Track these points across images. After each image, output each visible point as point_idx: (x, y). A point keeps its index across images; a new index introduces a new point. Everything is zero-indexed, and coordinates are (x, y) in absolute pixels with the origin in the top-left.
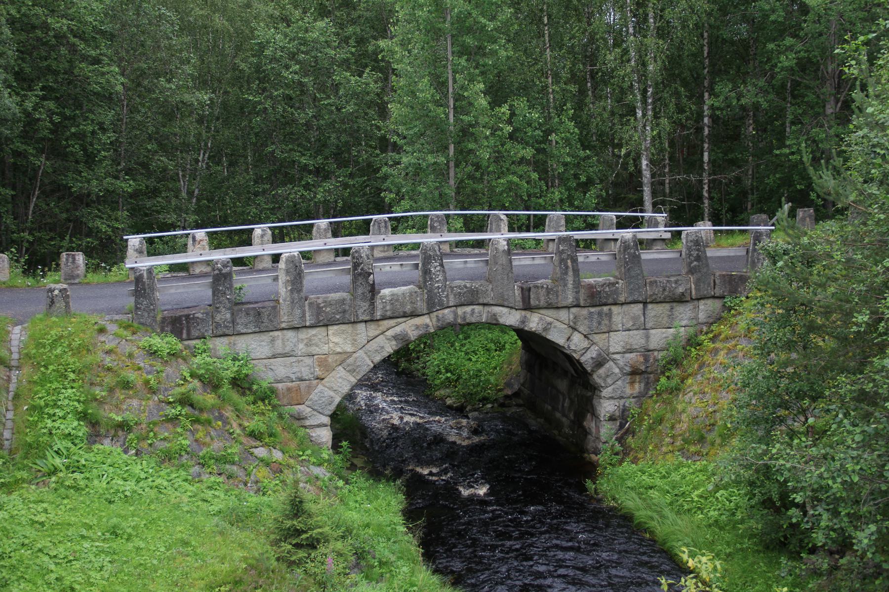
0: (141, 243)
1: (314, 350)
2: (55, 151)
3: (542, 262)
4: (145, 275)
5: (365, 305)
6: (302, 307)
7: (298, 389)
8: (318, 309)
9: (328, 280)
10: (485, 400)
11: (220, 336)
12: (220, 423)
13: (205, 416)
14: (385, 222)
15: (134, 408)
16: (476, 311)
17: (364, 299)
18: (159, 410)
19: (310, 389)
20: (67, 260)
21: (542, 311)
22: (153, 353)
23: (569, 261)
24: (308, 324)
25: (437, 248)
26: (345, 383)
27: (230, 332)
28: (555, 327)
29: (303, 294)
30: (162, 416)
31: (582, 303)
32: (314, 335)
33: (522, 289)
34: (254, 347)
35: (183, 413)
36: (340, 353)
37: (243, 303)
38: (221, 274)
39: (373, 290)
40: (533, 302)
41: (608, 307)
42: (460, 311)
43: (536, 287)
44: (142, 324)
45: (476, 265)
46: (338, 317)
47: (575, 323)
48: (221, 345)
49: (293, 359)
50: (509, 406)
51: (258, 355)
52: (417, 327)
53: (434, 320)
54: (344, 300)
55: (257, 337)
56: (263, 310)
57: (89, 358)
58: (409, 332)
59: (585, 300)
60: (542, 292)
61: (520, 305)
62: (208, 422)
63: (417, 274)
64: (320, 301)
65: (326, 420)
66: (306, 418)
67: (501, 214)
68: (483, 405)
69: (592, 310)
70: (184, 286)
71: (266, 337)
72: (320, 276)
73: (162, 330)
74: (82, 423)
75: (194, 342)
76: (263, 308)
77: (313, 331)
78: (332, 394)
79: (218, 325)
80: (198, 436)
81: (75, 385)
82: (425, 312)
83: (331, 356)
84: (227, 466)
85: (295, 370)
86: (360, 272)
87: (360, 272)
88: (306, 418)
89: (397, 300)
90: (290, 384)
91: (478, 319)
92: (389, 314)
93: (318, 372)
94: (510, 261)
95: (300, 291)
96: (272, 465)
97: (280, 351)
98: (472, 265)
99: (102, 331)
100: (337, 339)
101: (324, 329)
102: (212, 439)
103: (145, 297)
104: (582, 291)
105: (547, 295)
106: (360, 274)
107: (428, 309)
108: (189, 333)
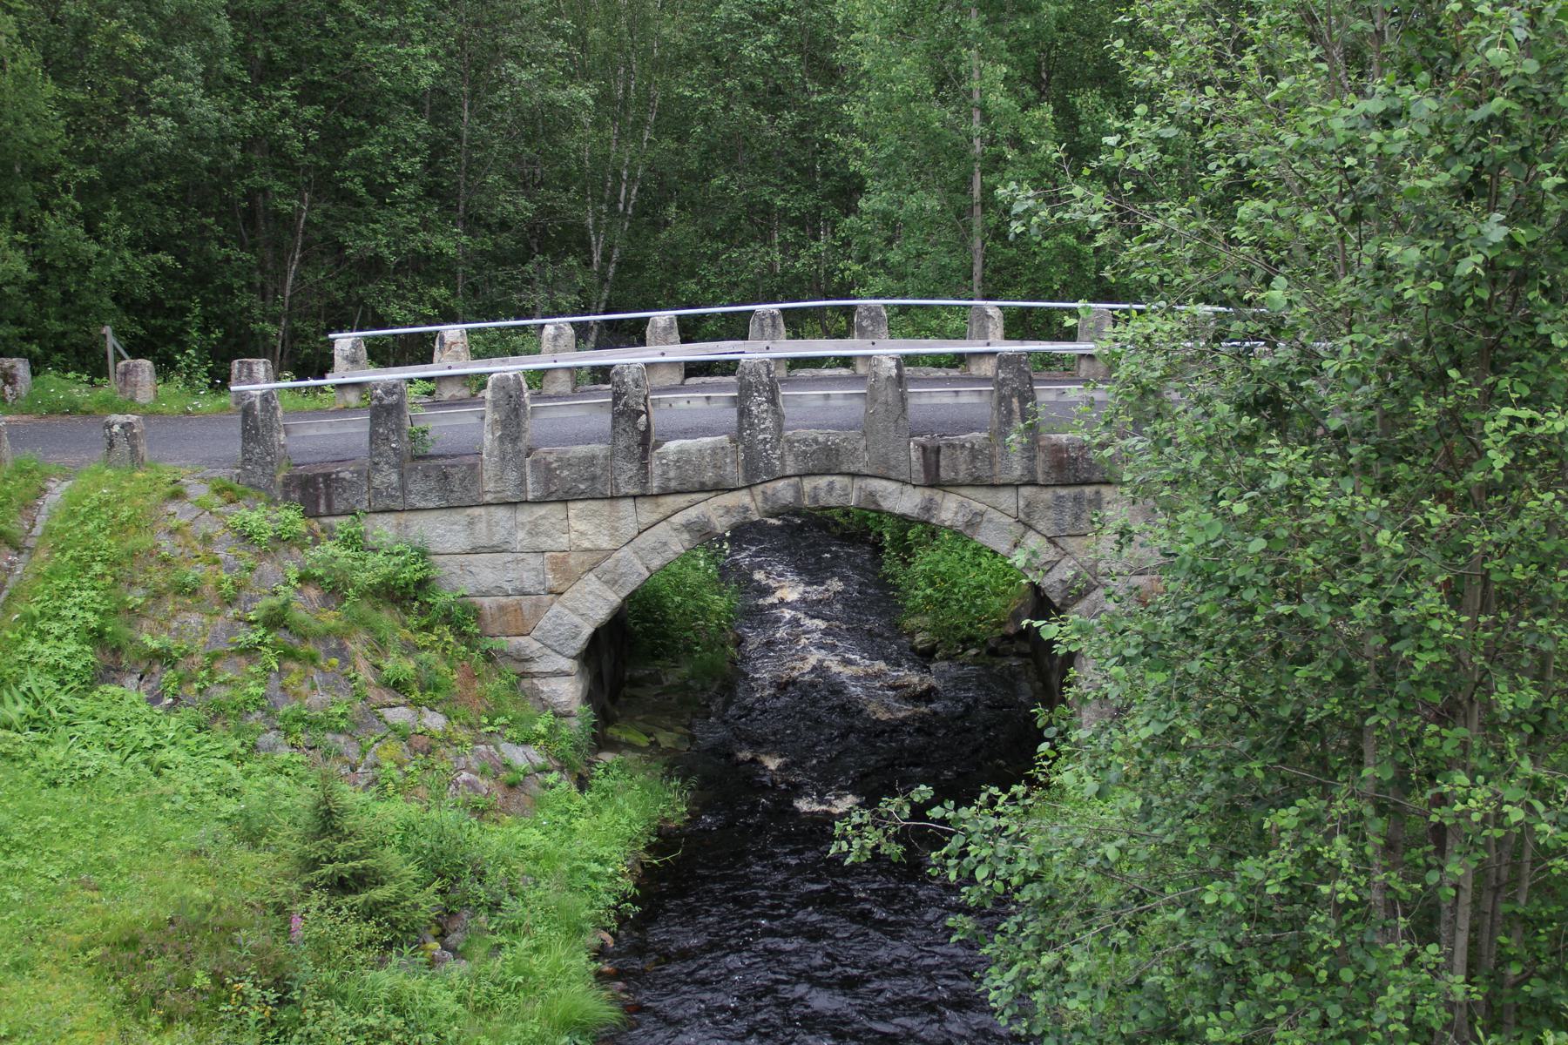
0: (355, 346)
1: (545, 542)
2: (325, 187)
3: (975, 399)
4: (258, 405)
5: (631, 468)
6: (520, 467)
7: (518, 609)
8: (547, 473)
9: (574, 425)
10: (969, 641)
11: (383, 512)
12: (335, 661)
13: (310, 647)
14: (773, 317)
15: (194, 628)
16: (837, 485)
17: (629, 456)
18: (229, 634)
19: (538, 610)
20: (240, 371)
21: (964, 491)
22: (246, 537)
23: (1015, 400)
24: (530, 497)
25: (763, 370)
26: (600, 603)
27: (397, 505)
28: (990, 521)
29: (522, 445)
30: (232, 644)
31: (1041, 479)
32: (543, 517)
33: (924, 448)
34: (442, 532)
35: (268, 640)
36: (587, 550)
37: (432, 457)
38: (382, 406)
39: (646, 443)
40: (945, 474)
41: (1093, 488)
42: (808, 484)
43: (951, 446)
44: (251, 485)
45: (848, 403)
46: (582, 487)
47: (1028, 515)
48: (383, 529)
49: (508, 557)
50: (1004, 655)
51: (448, 547)
52: (728, 511)
53: (759, 498)
54: (594, 457)
55: (445, 516)
56: (453, 470)
57: (143, 541)
58: (714, 519)
59: (1048, 474)
60: (963, 456)
61: (920, 477)
62: (313, 659)
63: (732, 415)
64: (551, 458)
65: (567, 664)
66: (530, 660)
67: (992, 307)
68: (965, 650)
69: (1063, 492)
70: (331, 425)
71: (461, 517)
72: (562, 415)
73: (286, 498)
74: (88, 648)
75: (335, 520)
76: (453, 466)
77: (541, 511)
78: (577, 620)
79: (378, 492)
80: (287, 681)
81: (99, 584)
82: (741, 483)
83: (573, 555)
84: (329, 736)
85: (511, 575)
86: (628, 415)
87: (628, 415)
88: (530, 660)
89: (688, 462)
90: (503, 600)
91: (842, 501)
92: (673, 484)
93: (551, 581)
94: (903, 399)
95: (515, 440)
96: (415, 738)
97: (483, 541)
98: (840, 403)
99: (177, 496)
100: (583, 526)
101: (559, 507)
102: (314, 688)
103: (258, 442)
104: (1041, 456)
105: (972, 461)
106: (621, 414)
107: (746, 479)
108: (329, 505)
